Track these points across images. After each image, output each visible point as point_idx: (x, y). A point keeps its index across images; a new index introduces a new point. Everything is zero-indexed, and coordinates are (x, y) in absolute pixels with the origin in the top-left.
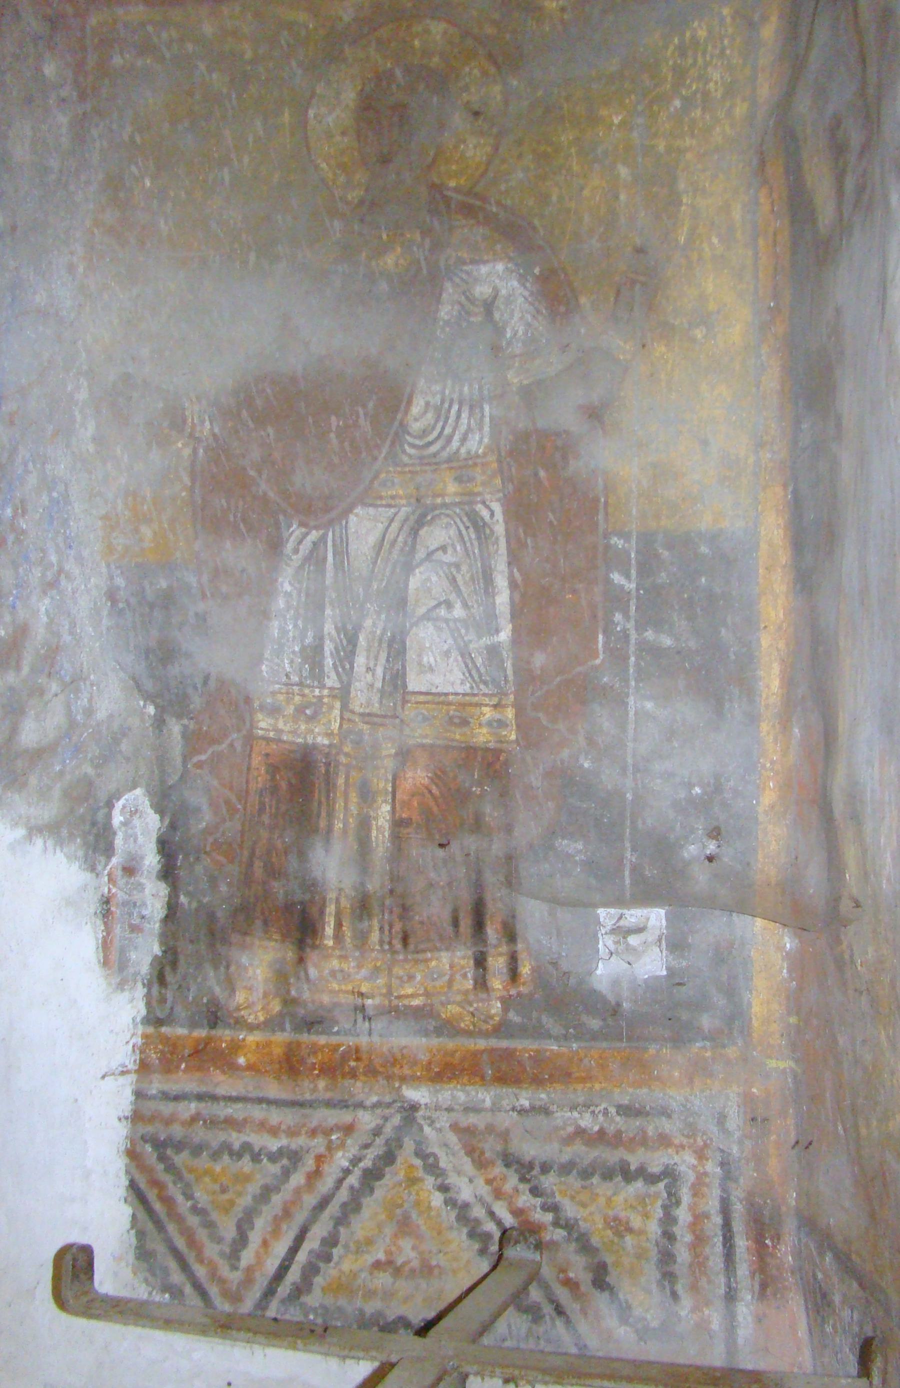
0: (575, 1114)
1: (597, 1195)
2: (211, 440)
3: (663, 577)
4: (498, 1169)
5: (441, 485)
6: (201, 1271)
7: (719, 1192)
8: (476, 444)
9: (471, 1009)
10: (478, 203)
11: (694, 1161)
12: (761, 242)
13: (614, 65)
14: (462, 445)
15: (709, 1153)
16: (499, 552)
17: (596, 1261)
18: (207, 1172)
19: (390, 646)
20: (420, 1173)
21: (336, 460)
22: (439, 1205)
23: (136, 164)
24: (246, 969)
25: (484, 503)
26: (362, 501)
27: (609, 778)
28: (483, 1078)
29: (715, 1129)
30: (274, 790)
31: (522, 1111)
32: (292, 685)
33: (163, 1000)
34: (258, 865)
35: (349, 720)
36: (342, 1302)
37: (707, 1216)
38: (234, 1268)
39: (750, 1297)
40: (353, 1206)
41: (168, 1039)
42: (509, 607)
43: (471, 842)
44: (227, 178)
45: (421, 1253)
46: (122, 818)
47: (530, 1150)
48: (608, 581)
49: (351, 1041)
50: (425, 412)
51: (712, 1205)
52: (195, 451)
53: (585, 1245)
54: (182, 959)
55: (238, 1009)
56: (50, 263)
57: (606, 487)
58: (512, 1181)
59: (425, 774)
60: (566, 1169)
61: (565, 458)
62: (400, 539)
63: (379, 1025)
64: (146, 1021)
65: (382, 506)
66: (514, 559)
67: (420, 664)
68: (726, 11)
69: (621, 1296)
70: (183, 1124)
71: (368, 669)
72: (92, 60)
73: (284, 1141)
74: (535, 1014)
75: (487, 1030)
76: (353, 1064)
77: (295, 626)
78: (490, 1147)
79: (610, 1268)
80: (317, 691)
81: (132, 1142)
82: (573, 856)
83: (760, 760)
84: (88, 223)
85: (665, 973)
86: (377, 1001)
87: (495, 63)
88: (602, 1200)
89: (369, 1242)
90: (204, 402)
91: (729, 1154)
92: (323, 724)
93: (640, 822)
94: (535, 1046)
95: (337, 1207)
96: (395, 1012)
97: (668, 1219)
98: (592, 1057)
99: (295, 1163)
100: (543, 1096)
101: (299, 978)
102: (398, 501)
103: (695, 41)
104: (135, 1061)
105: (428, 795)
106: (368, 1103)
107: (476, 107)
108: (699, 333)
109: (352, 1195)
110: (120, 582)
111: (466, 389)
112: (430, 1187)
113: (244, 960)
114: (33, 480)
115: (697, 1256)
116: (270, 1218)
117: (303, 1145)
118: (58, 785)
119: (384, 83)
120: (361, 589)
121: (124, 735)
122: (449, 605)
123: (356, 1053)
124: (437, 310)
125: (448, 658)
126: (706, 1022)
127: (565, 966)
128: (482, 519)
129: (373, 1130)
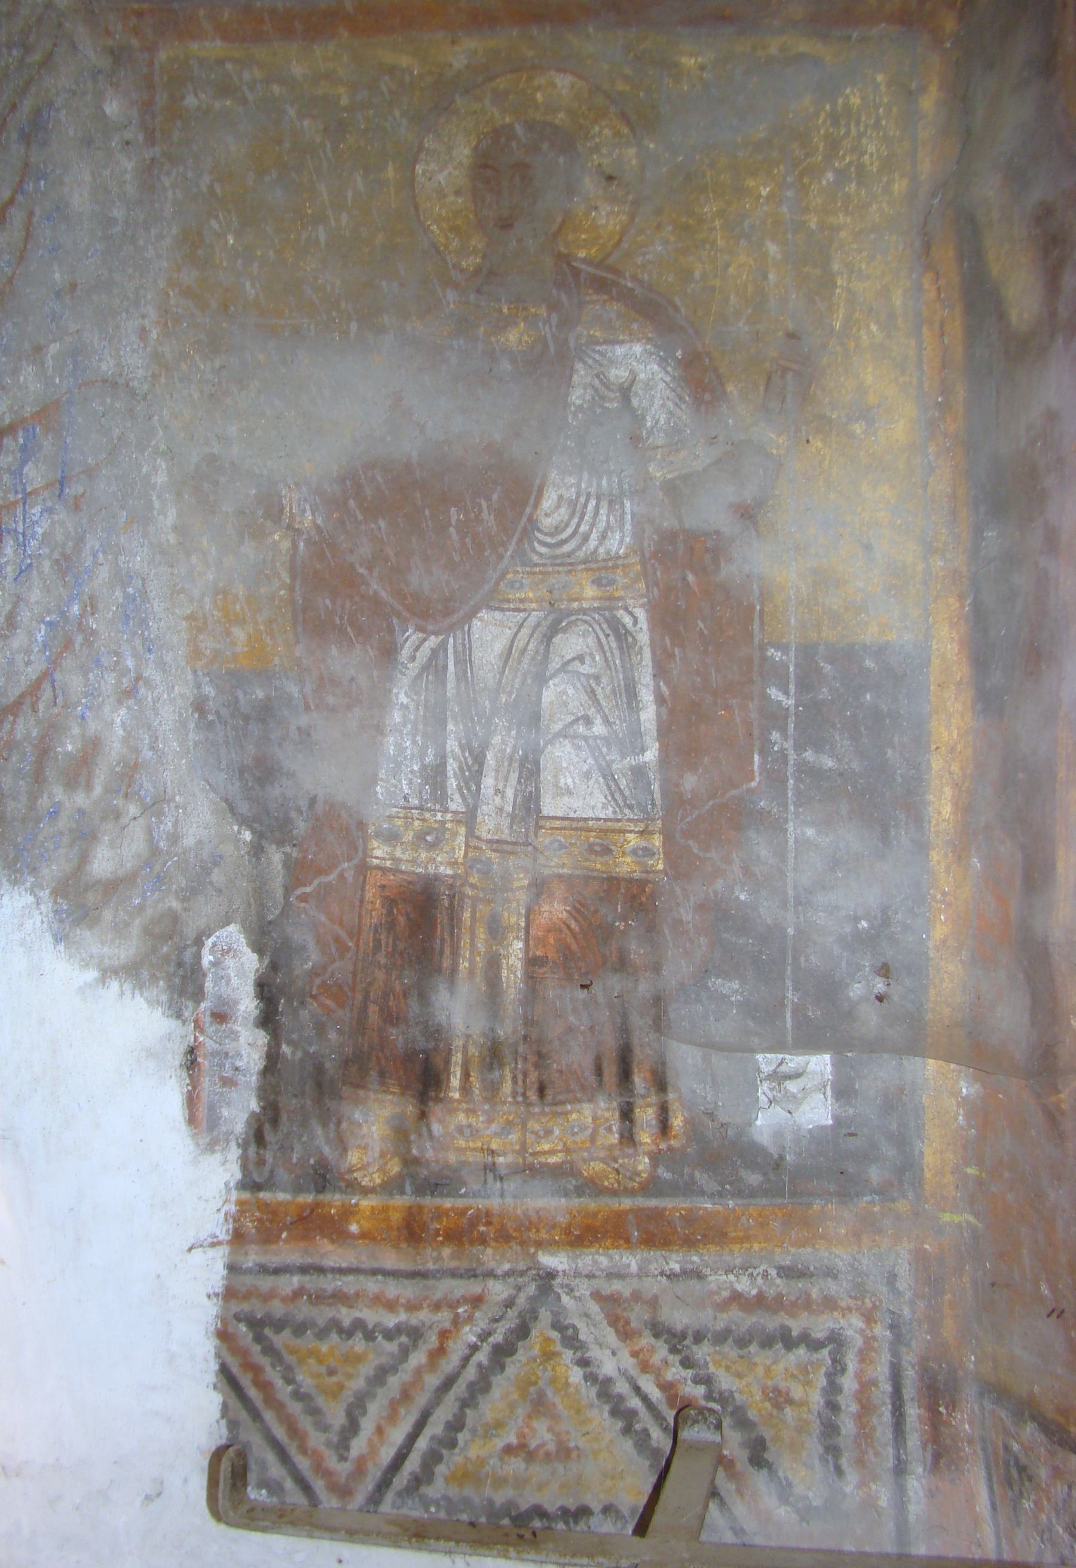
0: (731, 1277)
1: (755, 1364)
2: (313, 533)
3: (824, 694)
4: (646, 1340)
5: (577, 589)
6: (303, 1464)
7: (889, 1357)
8: (617, 543)
9: (616, 1166)
10: (610, 276)
11: (861, 1324)
12: (925, 331)
13: (760, 132)
14: (601, 544)
15: (878, 1314)
16: (644, 663)
17: (753, 1436)
18: (311, 1353)
19: (522, 766)
20: (558, 1347)
21: (457, 558)
22: (577, 1381)
23: (217, 217)
24: (360, 1125)
25: (626, 609)
27: (767, 911)
28: (628, 1241)
29: (885, 1289)
30: (391, 925)
31: (671, 1276)
32: (412, 808)
33: (261, 1162)
34: (373, 1009)
35: (475, 848)
36: (469, 1491)
37: (874, 1383)
38: (343, 1458)
39: (921, 1470)
40: (481, 1386)
41: (267, 1205)
42: (654, 723)
43: (615, 983)
44: (322, 238)
45: (557, 1435)
46: (211, 958)
47: (679, 1318)
48: (765, 697)
49: (481, 1203)
50: (558, 507)
51: (881, 1371)
52: (295, 545)
53: (742, 1422)
54: (284, 1117)
55: (351, 1171)
56: (118, 327)
57: (761, 595)
58: (661, 1352)
59: (562, 908)
60: (721, 1337)
61: (716, 561)
62: (531, 647)
63: (511, 1186)
64: (242, 1185)
65: (509, 610)
66: (660, 672)
67: (556, 785)
68: (880, 78)
69: (781, 1474)
70: (284, 1300)
71: (497, 791)
72: (161, 99)
73: (403, 1316)
74: (687, 1170)
75: (633, 1188)
76: (482, 1228)
77: (414, 742)
79: (768, 1444)
80: (439, 814)
81: (224, 1321)
82: (729, 997)
84: (162, 284)
85: (830, 1122)
86: (510, 1158)
87: (628, 122)
88: (760, 1370)
89: (499, 1425)
90: (304, 489)
91: (899, 1316)
92: (447, 852)
93: (802, 959)
94: (686, 1204)
95: (464, 1386)
96: (530, 1170)
97: (833, 1388)
98: (750, 1216)
99: (415, 1340)
100: (695, 1258)
101: (420, 1135)
102: (527, 605)
103: (847, 107)
104: (227, 1231)
105: (565, 930)
106: (499, 1272)
107: (608, 171)
108: (858, 428)
109: (481, 1373)
110: (209, 690)
111: (604, 482)
112: (568, 1361)
113: (358, 1116)
114: (104, 573)
115: (862, 1426)
116: (386, 1402)
117: (426, 1320)
118: (137, 922)
119: (503, 140)
120: (487, 703)
121: (216, 864)
122: (588, 721)
123: (487, 1216)
124: (567, 395)
125: (588, 779)
126: (875, 1174)
127: (723, 1117)
128: (624, 626)
129: (505, 1300)
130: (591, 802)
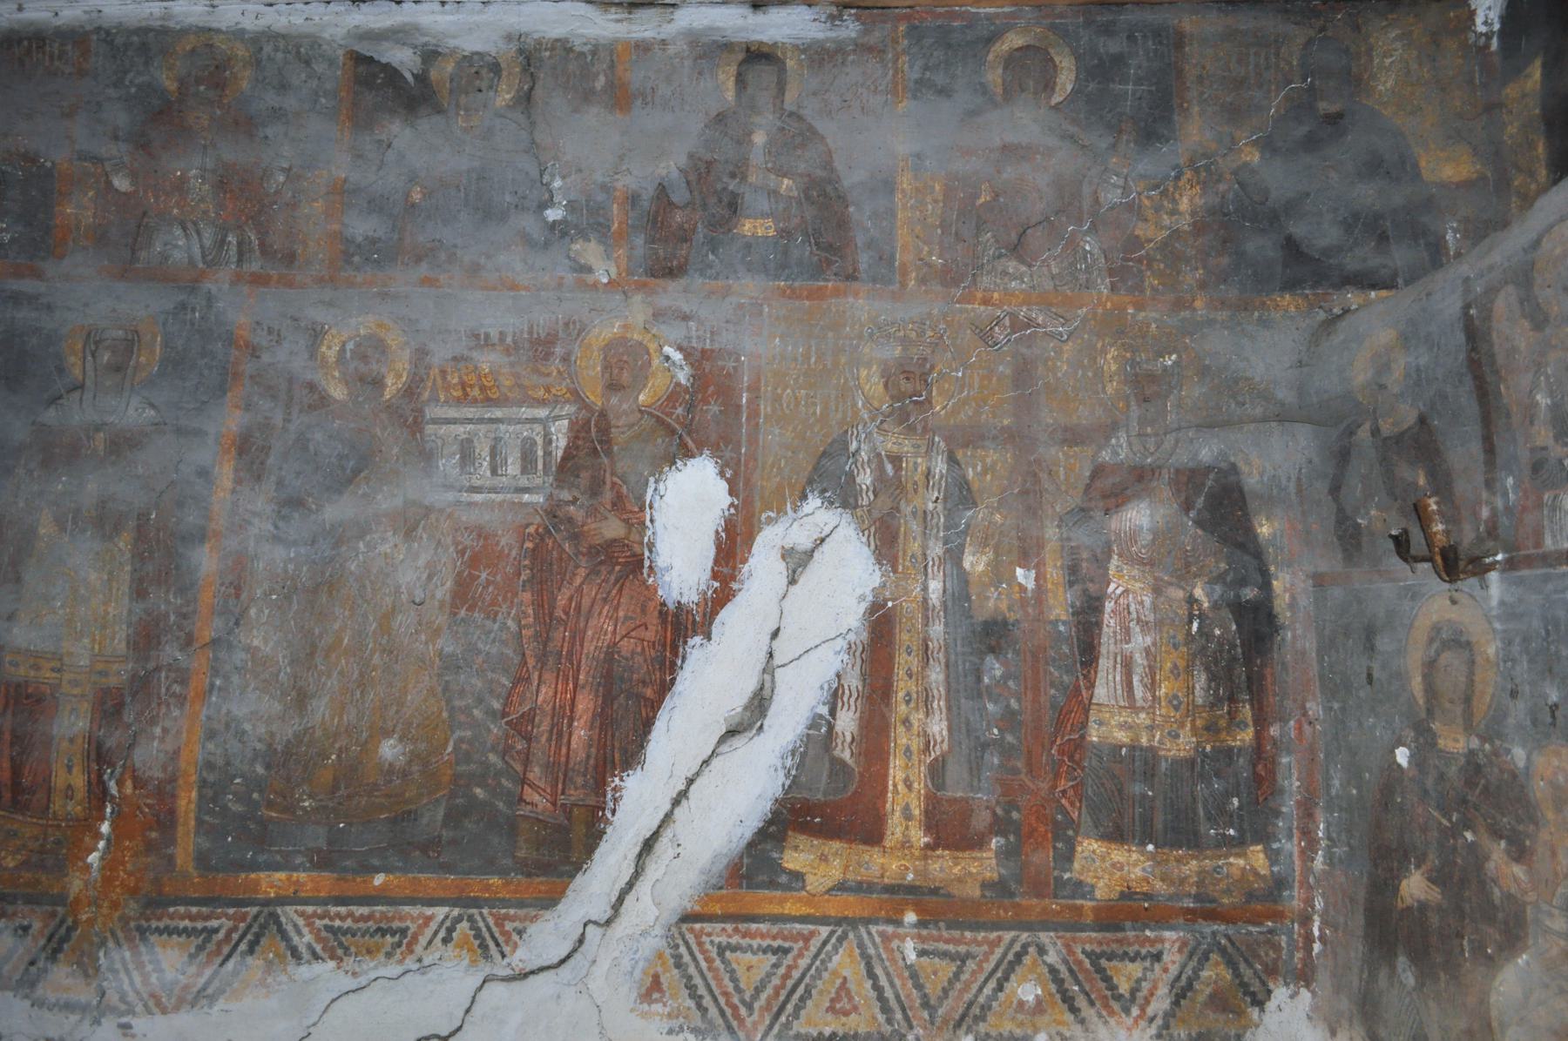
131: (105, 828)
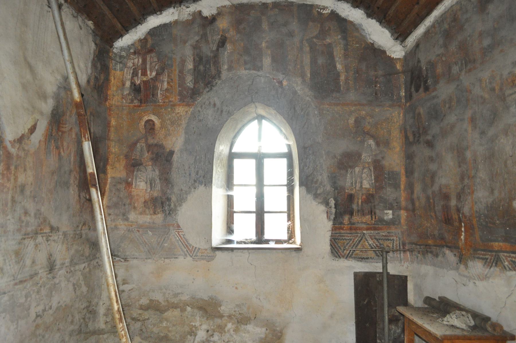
26: (357, 166)
27: (385, 197)
40: (358, 245)
43: (370, 204)
47: (377, 237)
51: (398, 243)
78: (373, 237)
83: (403, 195)
96: (362, 223)
97: (393, 245)
126: (397, 223)
130: (368, 186)
131: (463, 229)
